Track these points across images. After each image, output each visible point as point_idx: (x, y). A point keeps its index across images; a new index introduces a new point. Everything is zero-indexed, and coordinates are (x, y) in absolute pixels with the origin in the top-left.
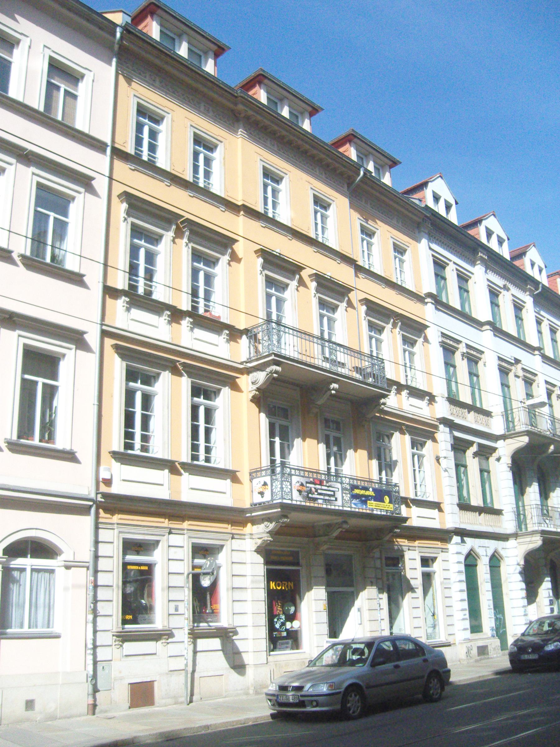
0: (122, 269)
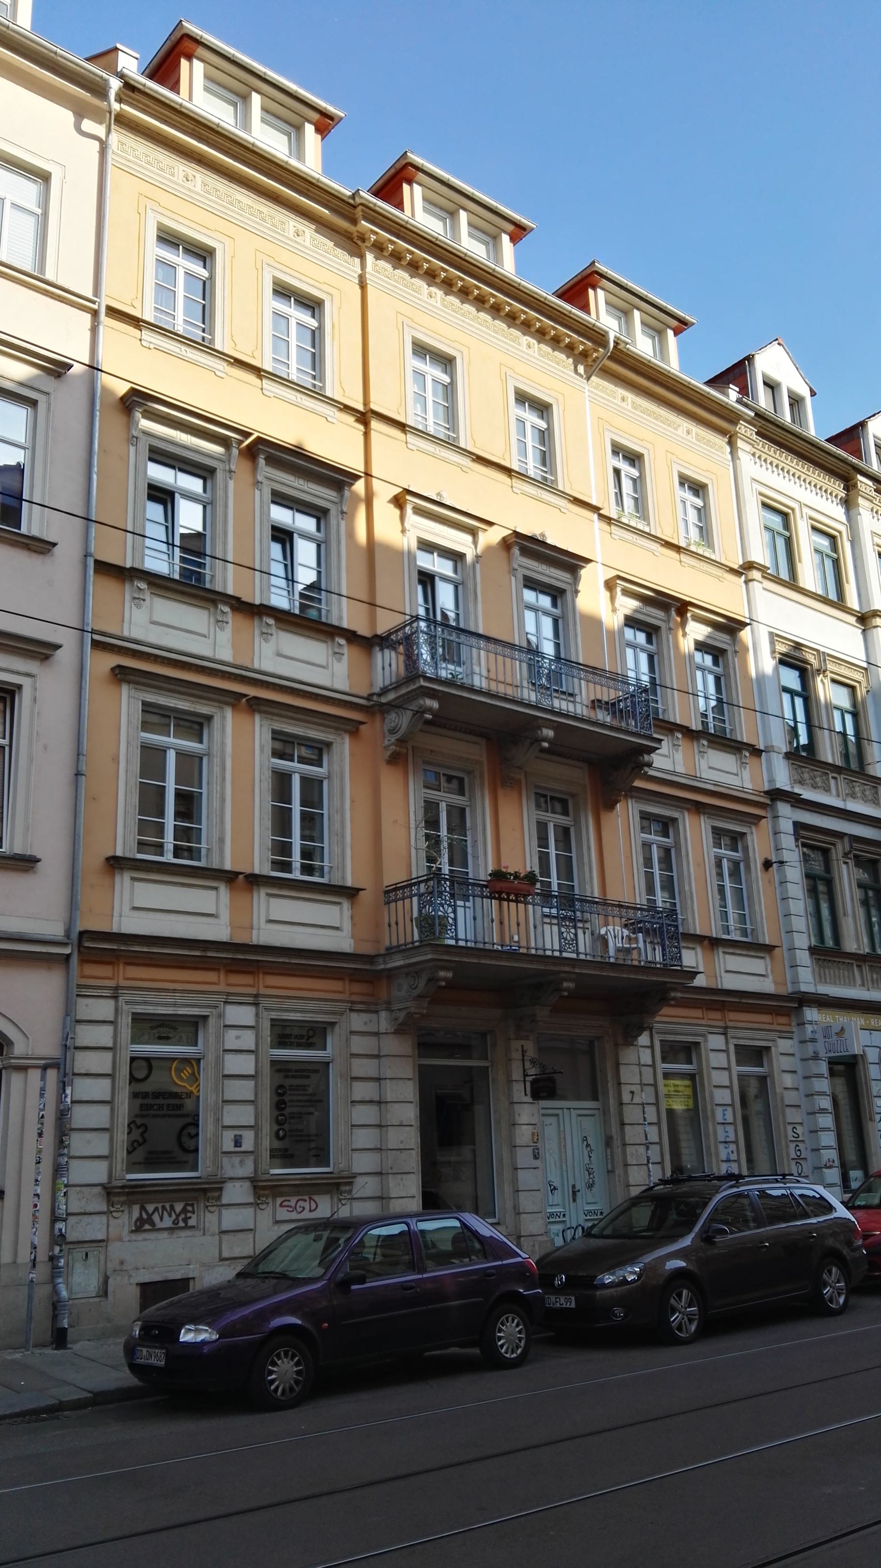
0: (147, 539)
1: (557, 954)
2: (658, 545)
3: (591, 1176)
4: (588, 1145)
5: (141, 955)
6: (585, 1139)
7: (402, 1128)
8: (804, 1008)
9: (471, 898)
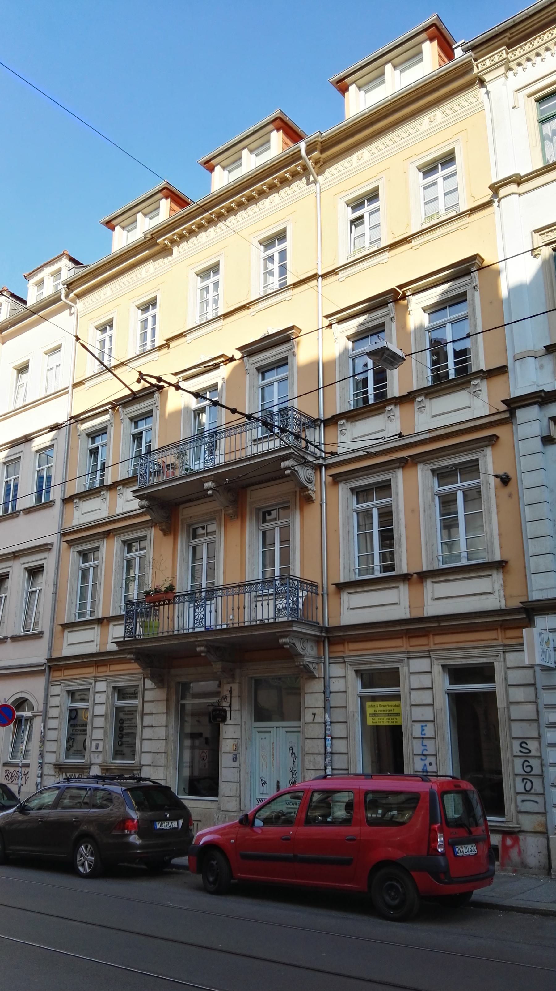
1: (191, 631)
2: (387, 253)
3: (294, 776)
4: (293, 753)
5: (71, 664)
6: (291, 748)
7: (159, 741)
8: (535, 617)
9: (215, 599)
